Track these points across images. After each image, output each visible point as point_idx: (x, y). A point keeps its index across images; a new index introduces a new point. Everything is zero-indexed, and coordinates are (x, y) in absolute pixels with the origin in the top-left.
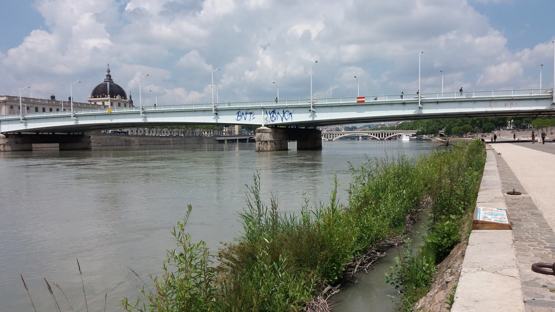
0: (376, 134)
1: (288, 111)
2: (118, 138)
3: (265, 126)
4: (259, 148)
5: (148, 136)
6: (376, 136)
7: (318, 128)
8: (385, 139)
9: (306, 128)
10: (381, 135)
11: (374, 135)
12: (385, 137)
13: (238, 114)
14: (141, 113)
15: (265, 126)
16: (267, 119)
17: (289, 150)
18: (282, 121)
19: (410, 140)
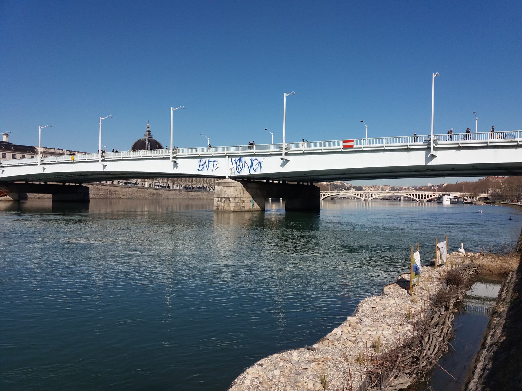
0: (416, 195)
1: (257, 160)
2: (145, 191)
3: (231, 178)
4: (218, 207)
5: (176, 190)
6: (416, 197)
7: (315, 184)
8: (425, 200)
9: (299, 183)
10: (421, 197)
11: (413, 195)
12: (425, 198)
13: (199, 162)
14: (100, 161)
15: (231, 178)
16: (232, 170)
17: (267, 211)
18: (250, 172)
19: (451, 203)
